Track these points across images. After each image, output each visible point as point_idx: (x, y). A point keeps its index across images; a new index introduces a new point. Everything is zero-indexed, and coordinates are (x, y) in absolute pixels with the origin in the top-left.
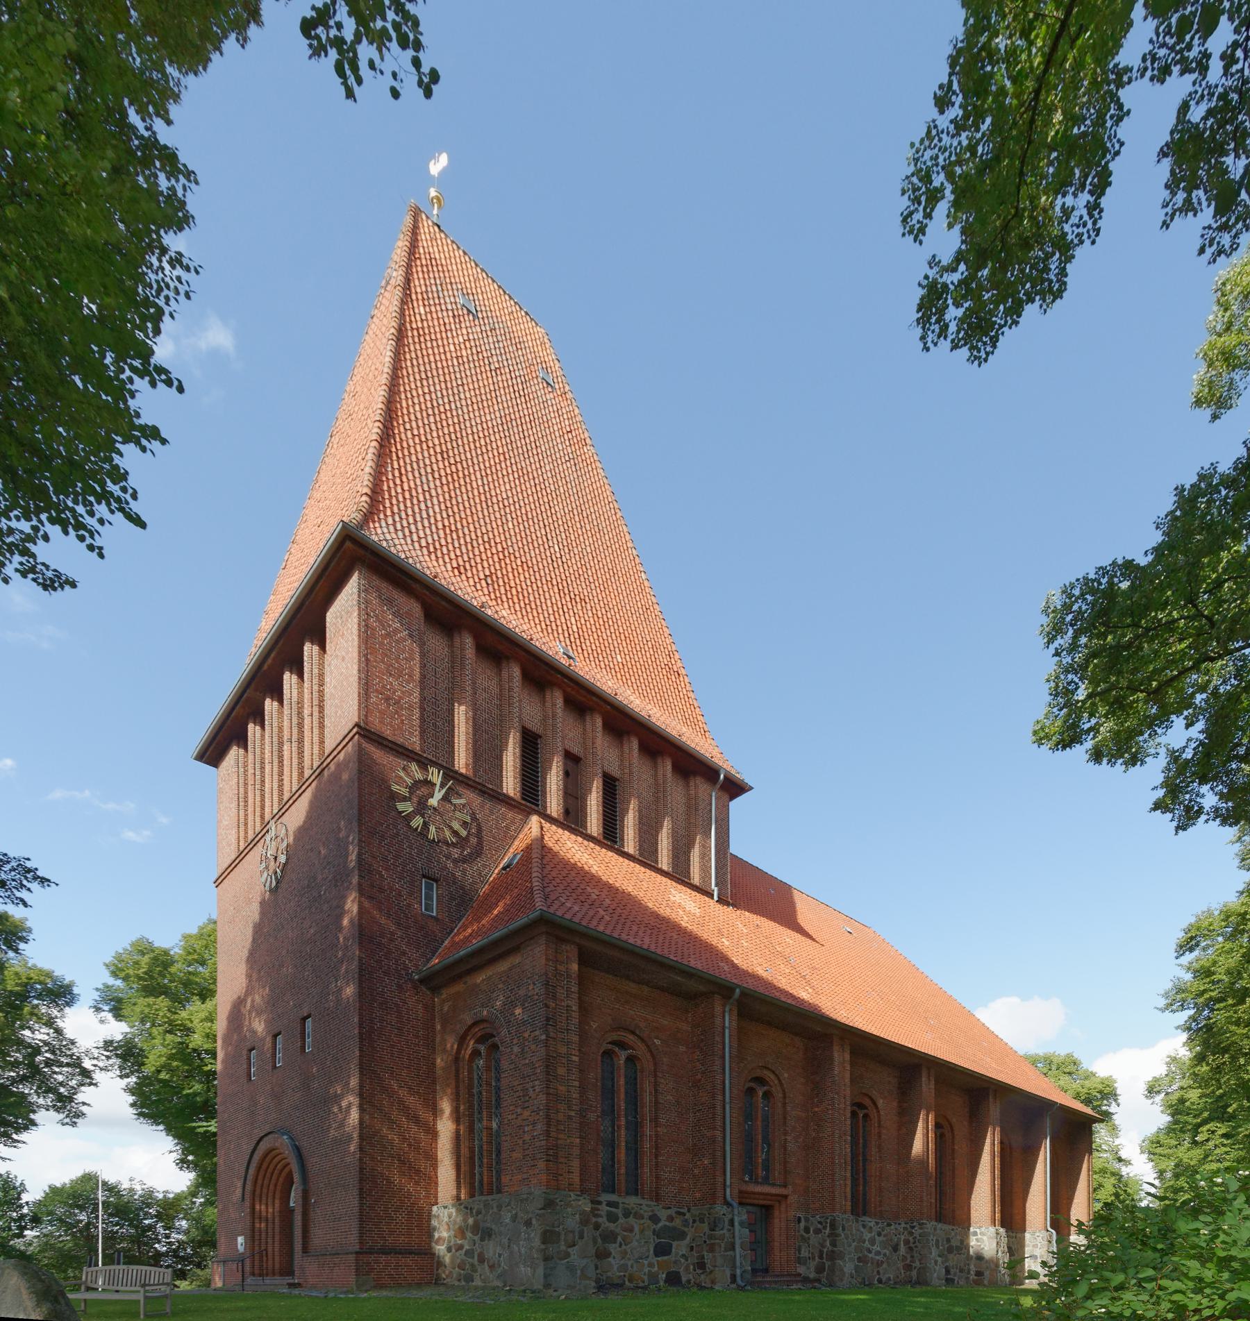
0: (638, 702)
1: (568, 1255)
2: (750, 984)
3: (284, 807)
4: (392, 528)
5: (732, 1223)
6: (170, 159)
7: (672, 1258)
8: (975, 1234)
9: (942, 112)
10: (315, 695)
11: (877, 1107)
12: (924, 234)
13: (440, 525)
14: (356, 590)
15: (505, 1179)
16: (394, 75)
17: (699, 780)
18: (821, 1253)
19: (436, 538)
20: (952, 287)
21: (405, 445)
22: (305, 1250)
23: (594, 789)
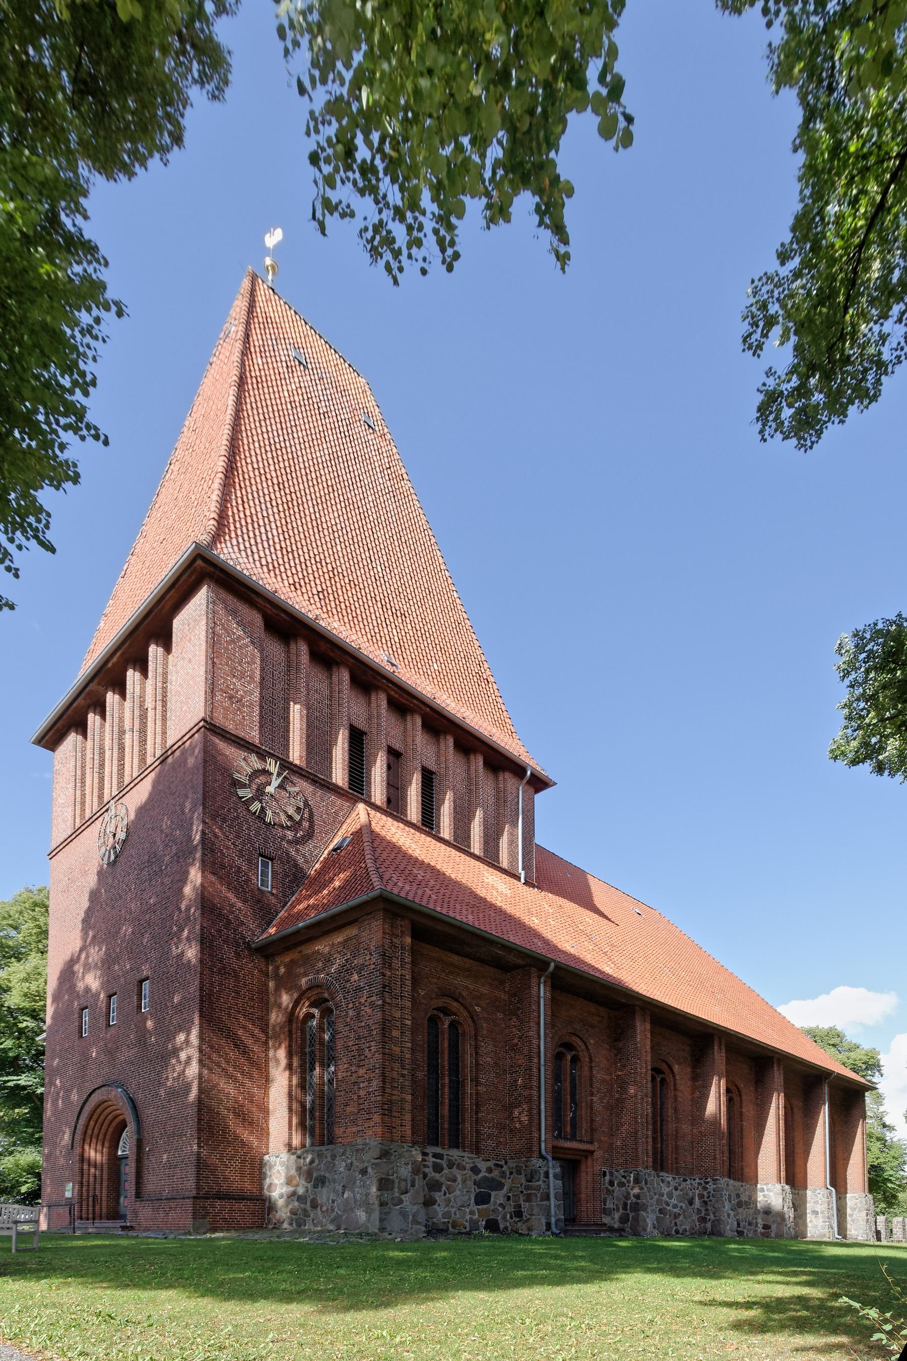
0: (453, 705)
1: (401, 1201)
2: (562, 959)
3: (124, 790)
4: (236, 548)
5: (547, 1175)
6: (90, 249)
7: (491, 1206)
8: (762, 1190)
9: (783, 264)
10: (159, 691)
11: (673, 1072)
12: (761, 350)
13: (278, 547)
14: (204, 602)
15: (338, 1131)
16: (424, 260)
17: (507, 775)
18: (625, 1204)
19: (274, 558)
20: (786, 393)
21: (246, 477)
22: (138, 1195)
23: (414, 781)
